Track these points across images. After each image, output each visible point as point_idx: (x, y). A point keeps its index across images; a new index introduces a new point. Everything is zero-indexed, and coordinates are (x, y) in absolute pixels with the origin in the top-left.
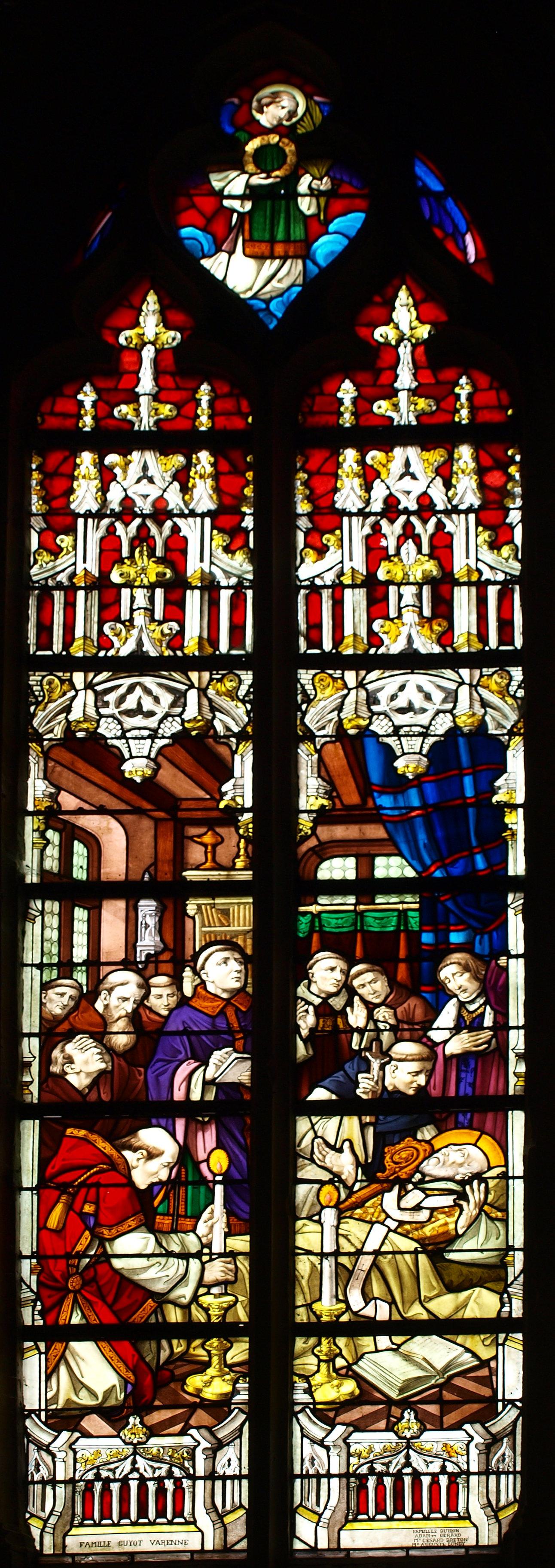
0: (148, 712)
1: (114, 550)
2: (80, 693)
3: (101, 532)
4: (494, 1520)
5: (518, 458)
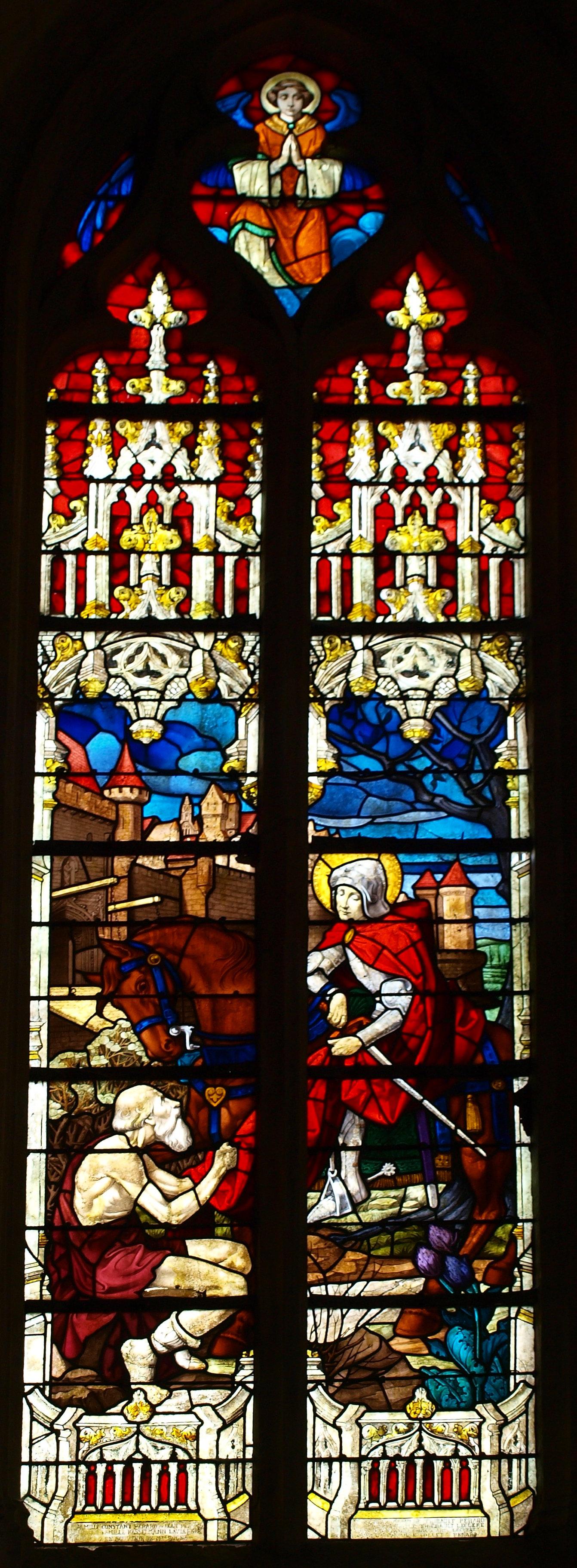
0: (153, 671)
1: (388, 518)
2: (359, 653)
3: (377, 499)
4: (506, 1509)
5: (521, 435)
